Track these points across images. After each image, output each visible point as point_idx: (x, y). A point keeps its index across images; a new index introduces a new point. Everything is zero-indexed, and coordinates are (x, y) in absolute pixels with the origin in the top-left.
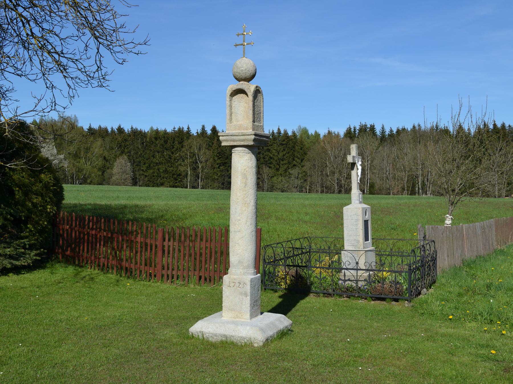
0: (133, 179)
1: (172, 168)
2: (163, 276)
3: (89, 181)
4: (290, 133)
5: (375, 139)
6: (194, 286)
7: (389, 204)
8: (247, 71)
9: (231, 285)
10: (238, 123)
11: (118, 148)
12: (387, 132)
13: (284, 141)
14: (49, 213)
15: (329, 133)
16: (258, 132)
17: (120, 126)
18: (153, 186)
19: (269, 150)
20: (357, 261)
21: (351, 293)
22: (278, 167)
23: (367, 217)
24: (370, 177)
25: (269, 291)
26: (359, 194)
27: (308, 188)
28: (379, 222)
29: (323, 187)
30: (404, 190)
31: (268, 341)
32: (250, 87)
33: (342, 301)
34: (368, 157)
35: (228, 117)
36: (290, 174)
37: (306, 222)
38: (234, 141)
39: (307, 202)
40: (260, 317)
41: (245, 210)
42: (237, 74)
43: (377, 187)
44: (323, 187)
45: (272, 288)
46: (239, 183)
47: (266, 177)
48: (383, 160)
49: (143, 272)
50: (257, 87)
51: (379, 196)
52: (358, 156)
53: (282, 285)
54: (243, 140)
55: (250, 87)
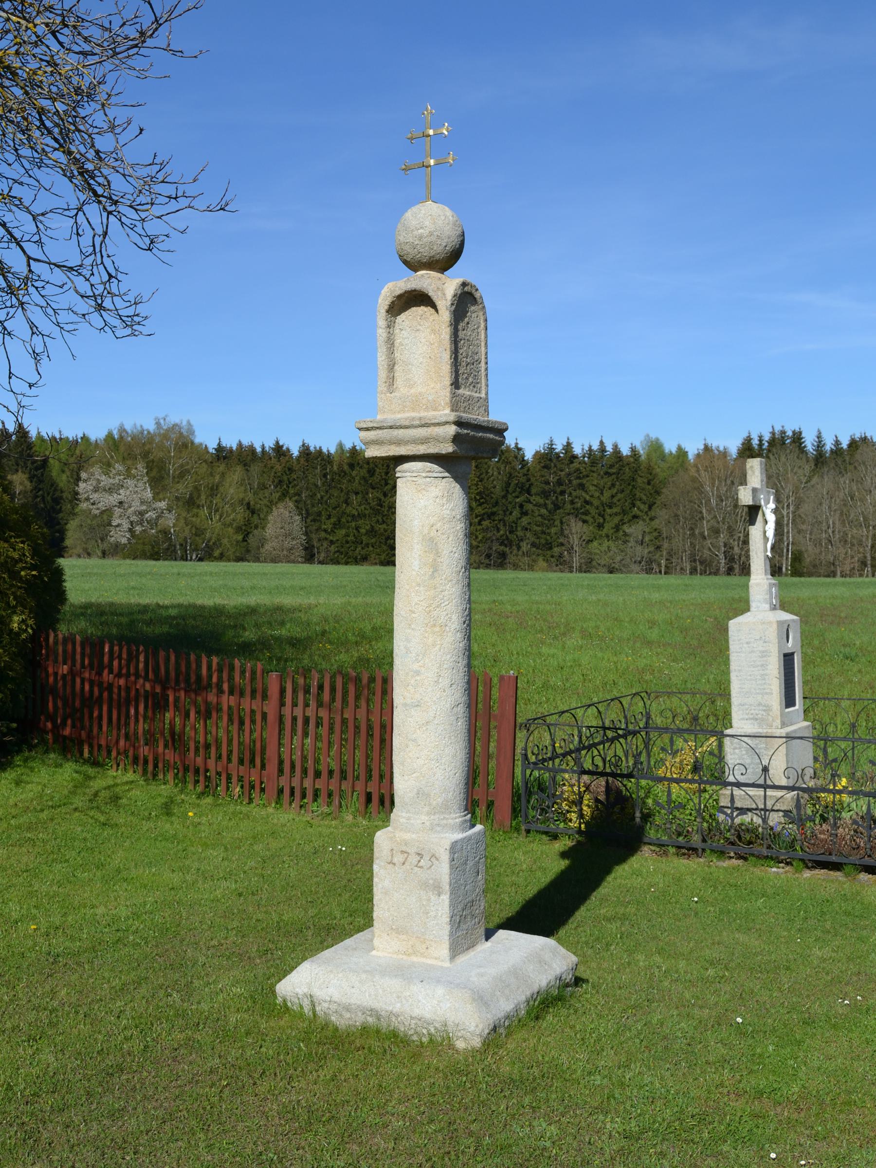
0: (306, 549)
1: (384, 526)
2: (281, 791)
3: (217, 553)
4: (625, 451)
5: (804, 459)
6: (355, 817)
7: (834, 597)
8: (433, 238)
9: (395, 860)
10: (413, 391)
11: (276, 487)
12: (829, 445)
13: (611, 466)
14: (18, 634)
15: (707, 448)
16: (465, 416)
17: (277, 442)
18: (347, 563)
19: (582, 486)
20: (765, 762)
21: (748, 844)
22: (601, 520)
23: (790, 644)
24: (793, 539)
25: (538, 836)
26: (771, 586)
27: (663, 562)
28: (816, 642)
29: (695, 561)
30: (866, 566)
31: (496, 1036)
32: (444, 287)
33: (726, 869)
34: (788, 497)
35: (382, 374)
36: (626, 534)
37: (649, 643)
38: (399, 442)
39: (656, 596)
40: (486, 946)
41: (434, 645)
42: (407, 248)
43: (807, 560)
44: (695, 561)
45: (542, 827)
46: (416, 564)
47: (576, 542)
48: (821, 504)
49: (234, 779)
50: (464, 284)
51: (813, 580)
52: (765, 488)
53: (571, 820)
54: (424, 441)
55: (444, 287)
